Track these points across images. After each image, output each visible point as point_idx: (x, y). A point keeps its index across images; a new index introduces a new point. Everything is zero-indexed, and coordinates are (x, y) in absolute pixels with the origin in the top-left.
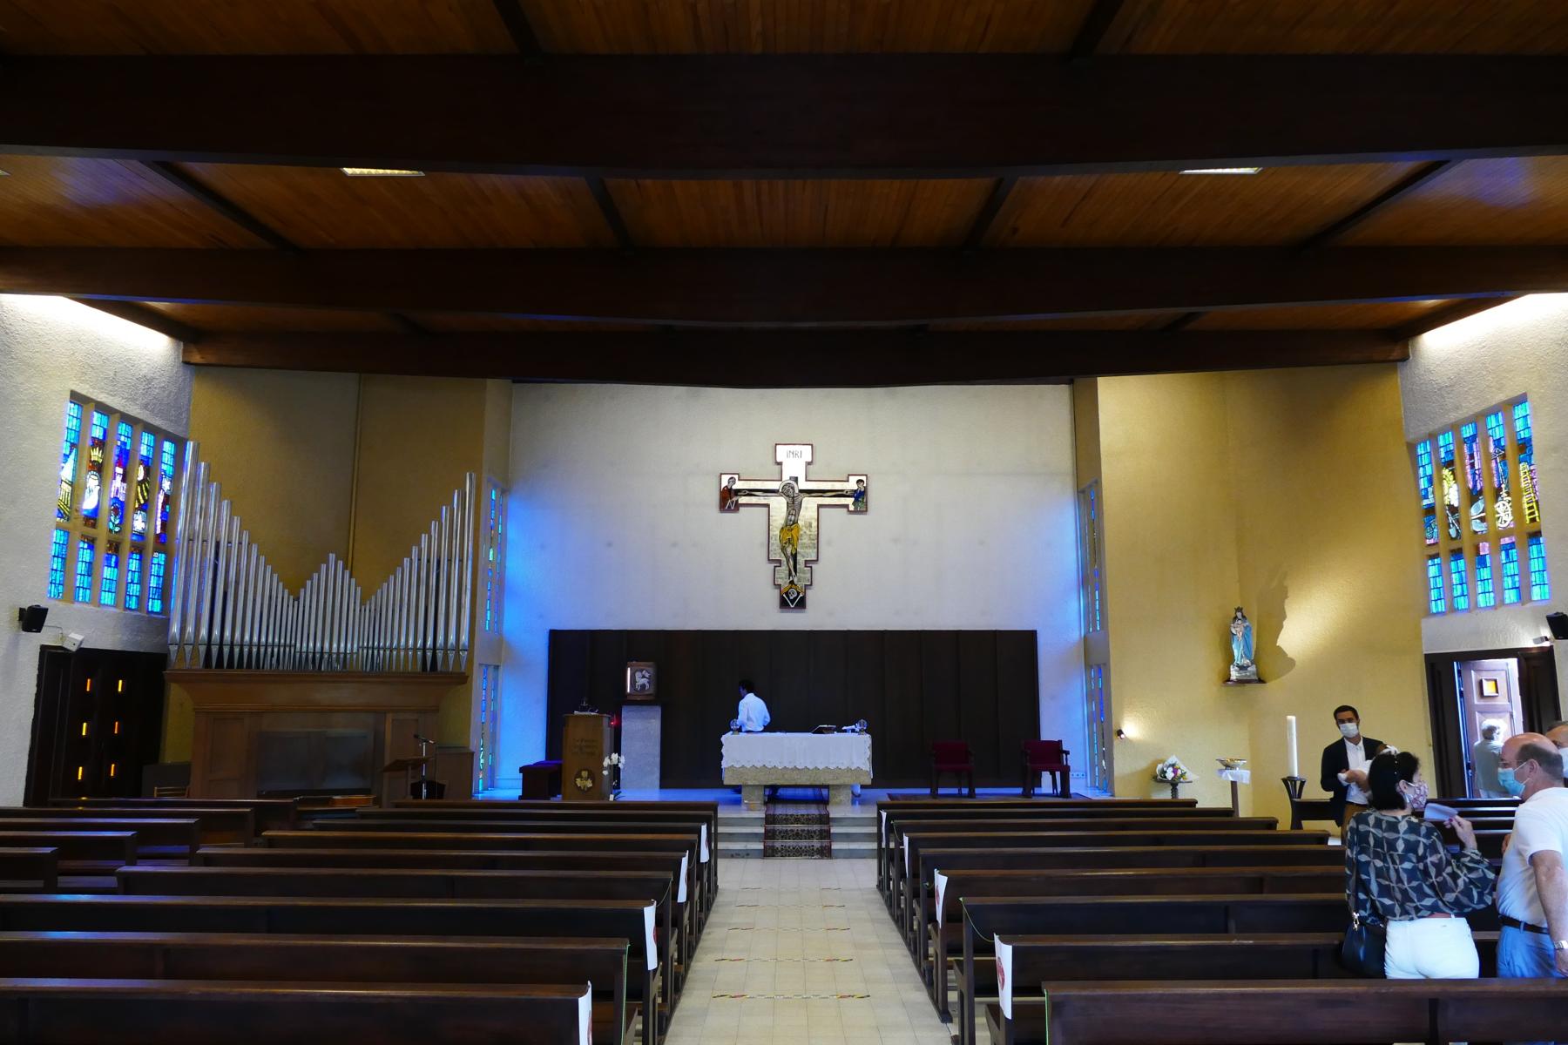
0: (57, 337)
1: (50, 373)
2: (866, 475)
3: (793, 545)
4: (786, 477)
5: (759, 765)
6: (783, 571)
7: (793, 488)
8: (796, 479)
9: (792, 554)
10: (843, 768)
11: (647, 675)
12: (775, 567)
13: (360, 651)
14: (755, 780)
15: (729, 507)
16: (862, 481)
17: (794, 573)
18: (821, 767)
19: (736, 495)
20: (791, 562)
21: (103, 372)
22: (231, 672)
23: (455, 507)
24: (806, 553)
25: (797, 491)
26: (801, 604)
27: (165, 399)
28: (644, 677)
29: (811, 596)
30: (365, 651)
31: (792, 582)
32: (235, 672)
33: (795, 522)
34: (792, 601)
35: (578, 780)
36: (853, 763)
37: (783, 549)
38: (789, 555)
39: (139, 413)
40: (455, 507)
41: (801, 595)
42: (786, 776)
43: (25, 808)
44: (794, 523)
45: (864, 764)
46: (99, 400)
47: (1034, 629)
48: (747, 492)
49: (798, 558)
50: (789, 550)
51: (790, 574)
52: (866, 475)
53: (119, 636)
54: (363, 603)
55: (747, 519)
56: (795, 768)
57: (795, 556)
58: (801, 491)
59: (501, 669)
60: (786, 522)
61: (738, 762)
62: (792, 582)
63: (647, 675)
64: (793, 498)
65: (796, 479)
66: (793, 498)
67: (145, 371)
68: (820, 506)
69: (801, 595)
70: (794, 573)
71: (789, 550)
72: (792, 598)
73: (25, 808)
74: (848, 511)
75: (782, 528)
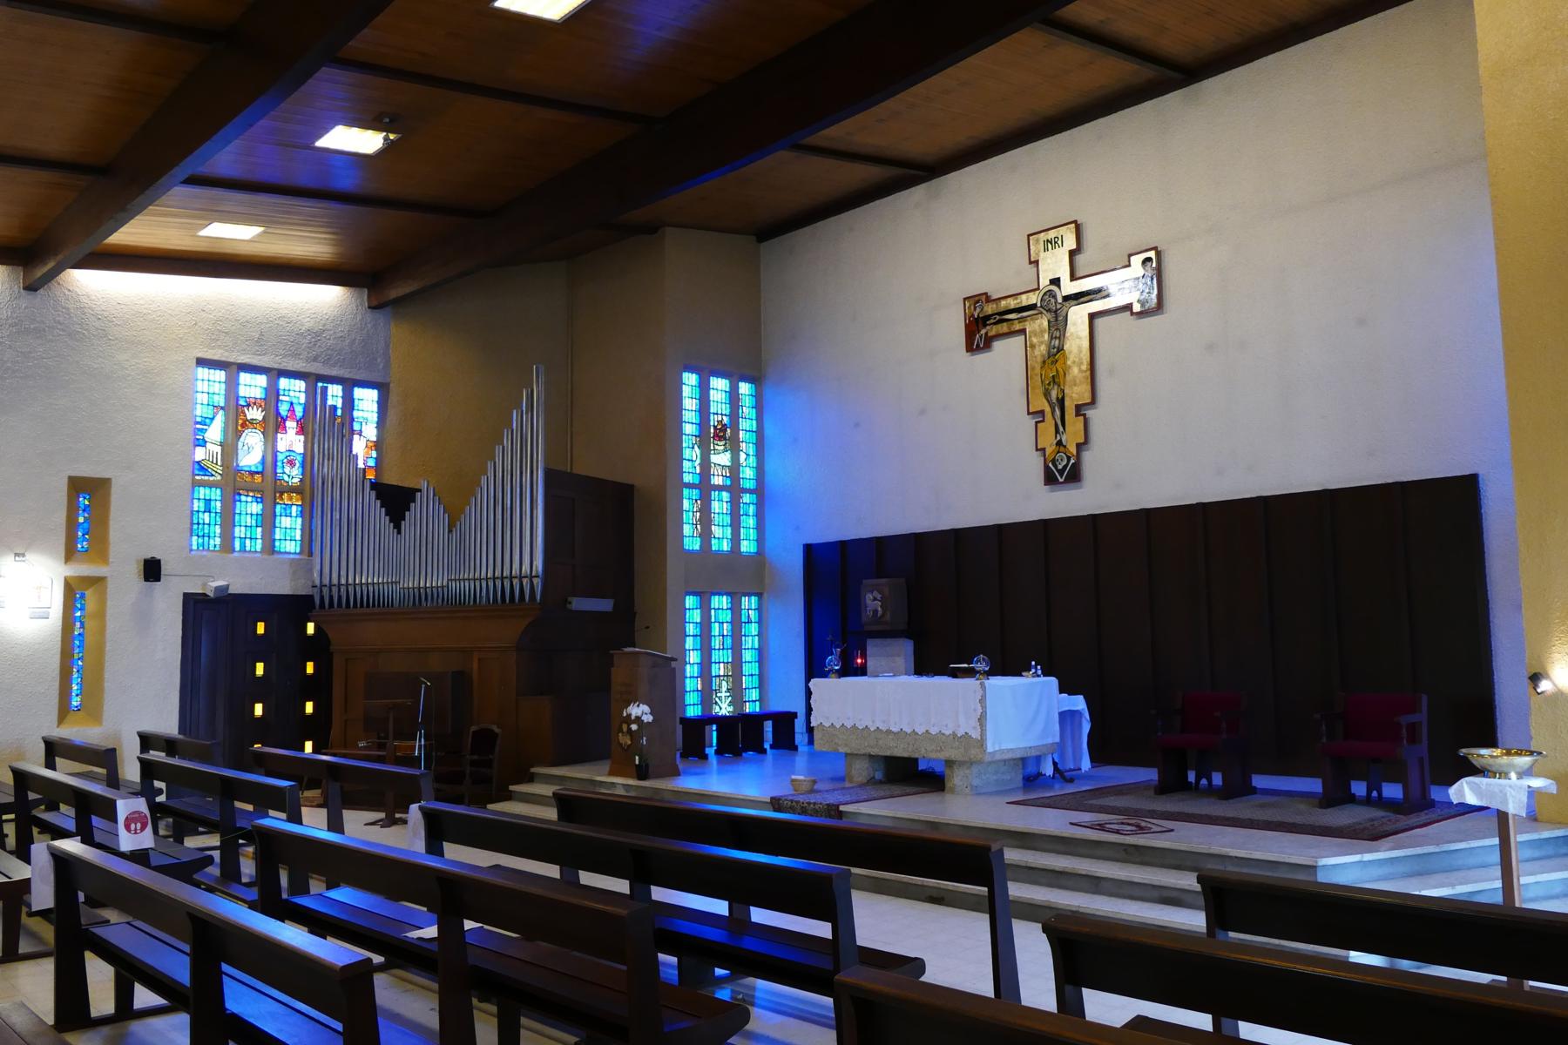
0: (170, 312)
1: (164, 346)
2: (1155, 248)
3: (1059, 386)
4: (1044, 282)
5: (849, 724)
6: (1048, 427)
7: (1055, 297)
8: (1056, 282)
9: (1058, 398)
10: (947, 733)
11: (879, 596)
12: (1037, 423)
13: (450, 583)
14: (846, 745)
15: (978, 345)
16: (1149, 259)
17: (1061, 429)
18: (920, 730)
19: (985, 325)
20: (1058, 412)
21: (242, 336)
22: (355, 611)
23: (524, 409)
24: (1077, 393)
25: (1060, 300)
26: (1074, 475)
27: (347, 348)
28: (875, 599)
29: (1090, 461)
30: (478, 583)
31: (1059, 443)
32: (359, 610)
33: (1060, 349)
34: (1061, 472)
35: (620, 734)
36: (959, 726)
37: (1047, 394)
38: (1054, 401)
39: (303, 367)
40: (524, 409)
41: (1072, 461)
42: (880, 742)
43: (181, 737)
44: (1058, 352)
45: (974, 728)
46: (239, 362)
47: (66, 481)
48: (998, 317)
49: (1067, 403)
50: (1054, 394)
51: (1057, 431)
52: (1155, 248)
53: (303, 581)
54: (450, 531)
55: (1008, 354)
56: (889, 732)
57: (1061, 402)
58: (1066, 298)
59: (765, 595)
60: (1049, 352)
61: (827, 718)
62: (1059, 443)
63: (879, 596)
64: (1056, 311)
65: (1056, 282)
66: (1056, 311)
67: (307, 326)
68: (1092, 317)
69: (1072, 461)
70: (1061, 429)
71: (1054, 394)
72: (1060, 467)
73: (181, 737)
74: (1132, 313)
75: (1044, 362)
